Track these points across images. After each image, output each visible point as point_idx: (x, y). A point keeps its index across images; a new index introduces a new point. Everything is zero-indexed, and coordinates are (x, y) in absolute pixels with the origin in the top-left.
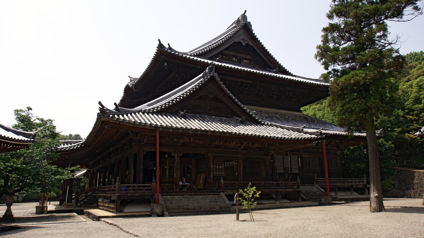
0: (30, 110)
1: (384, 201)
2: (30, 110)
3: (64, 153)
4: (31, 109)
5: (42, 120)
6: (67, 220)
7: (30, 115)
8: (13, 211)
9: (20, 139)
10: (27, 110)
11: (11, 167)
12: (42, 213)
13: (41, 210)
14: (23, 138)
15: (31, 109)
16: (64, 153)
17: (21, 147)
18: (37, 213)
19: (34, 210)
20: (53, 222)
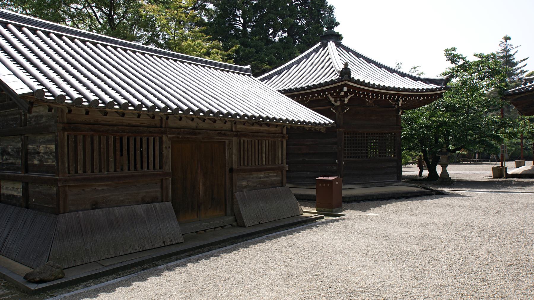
0: (508, 41)
1: (492, 175)
2: (508, 41)
3: (526, 94)
4: (509, 39)
5: (481, 56)
6: (518, 189)
7: (508, 47)
8: (449, 172)
9: (421, 88)
10: (504, 41)
11: (437, 121)
12: (501, 176)
13: (500, 172)
14: (434, 86)
15: (509, 39)
16: (526, 94)
17: (435, 97)
18: (495, 176)
19: (491, 173)
20: (486, 190)
